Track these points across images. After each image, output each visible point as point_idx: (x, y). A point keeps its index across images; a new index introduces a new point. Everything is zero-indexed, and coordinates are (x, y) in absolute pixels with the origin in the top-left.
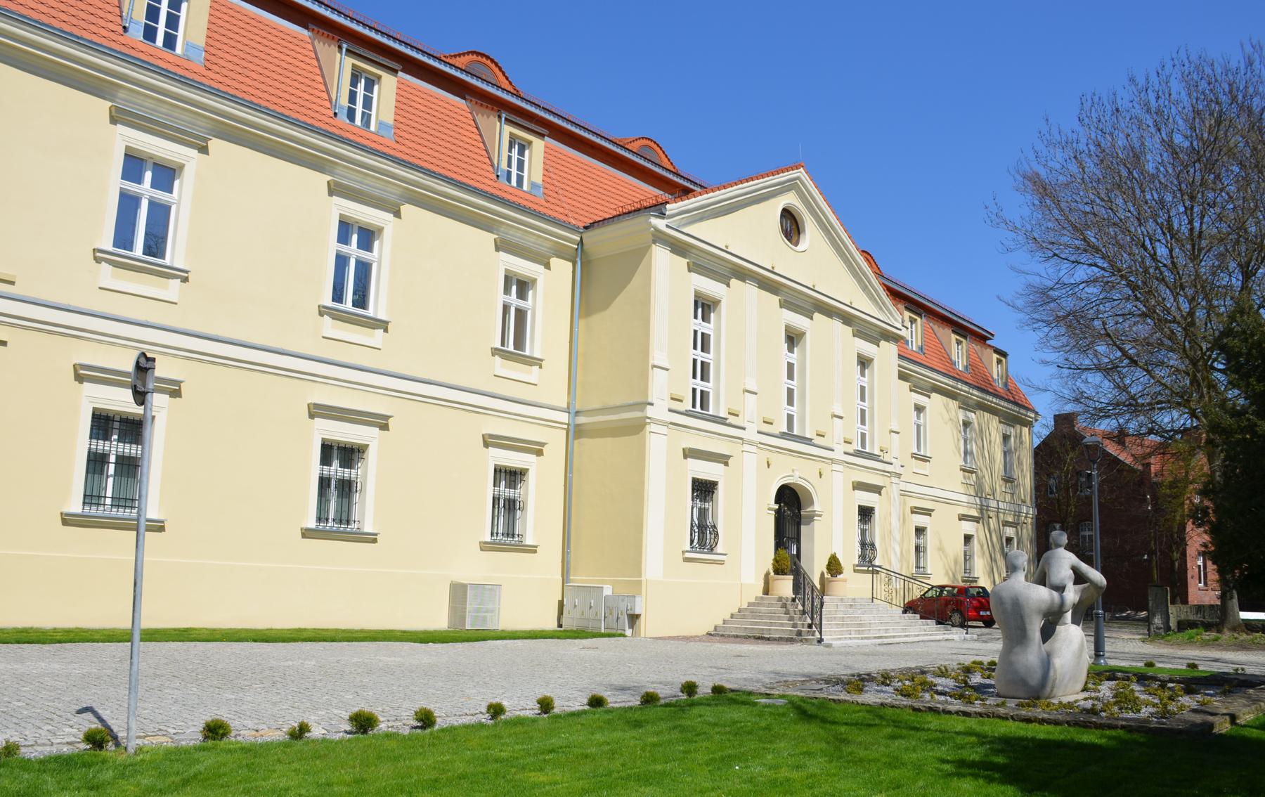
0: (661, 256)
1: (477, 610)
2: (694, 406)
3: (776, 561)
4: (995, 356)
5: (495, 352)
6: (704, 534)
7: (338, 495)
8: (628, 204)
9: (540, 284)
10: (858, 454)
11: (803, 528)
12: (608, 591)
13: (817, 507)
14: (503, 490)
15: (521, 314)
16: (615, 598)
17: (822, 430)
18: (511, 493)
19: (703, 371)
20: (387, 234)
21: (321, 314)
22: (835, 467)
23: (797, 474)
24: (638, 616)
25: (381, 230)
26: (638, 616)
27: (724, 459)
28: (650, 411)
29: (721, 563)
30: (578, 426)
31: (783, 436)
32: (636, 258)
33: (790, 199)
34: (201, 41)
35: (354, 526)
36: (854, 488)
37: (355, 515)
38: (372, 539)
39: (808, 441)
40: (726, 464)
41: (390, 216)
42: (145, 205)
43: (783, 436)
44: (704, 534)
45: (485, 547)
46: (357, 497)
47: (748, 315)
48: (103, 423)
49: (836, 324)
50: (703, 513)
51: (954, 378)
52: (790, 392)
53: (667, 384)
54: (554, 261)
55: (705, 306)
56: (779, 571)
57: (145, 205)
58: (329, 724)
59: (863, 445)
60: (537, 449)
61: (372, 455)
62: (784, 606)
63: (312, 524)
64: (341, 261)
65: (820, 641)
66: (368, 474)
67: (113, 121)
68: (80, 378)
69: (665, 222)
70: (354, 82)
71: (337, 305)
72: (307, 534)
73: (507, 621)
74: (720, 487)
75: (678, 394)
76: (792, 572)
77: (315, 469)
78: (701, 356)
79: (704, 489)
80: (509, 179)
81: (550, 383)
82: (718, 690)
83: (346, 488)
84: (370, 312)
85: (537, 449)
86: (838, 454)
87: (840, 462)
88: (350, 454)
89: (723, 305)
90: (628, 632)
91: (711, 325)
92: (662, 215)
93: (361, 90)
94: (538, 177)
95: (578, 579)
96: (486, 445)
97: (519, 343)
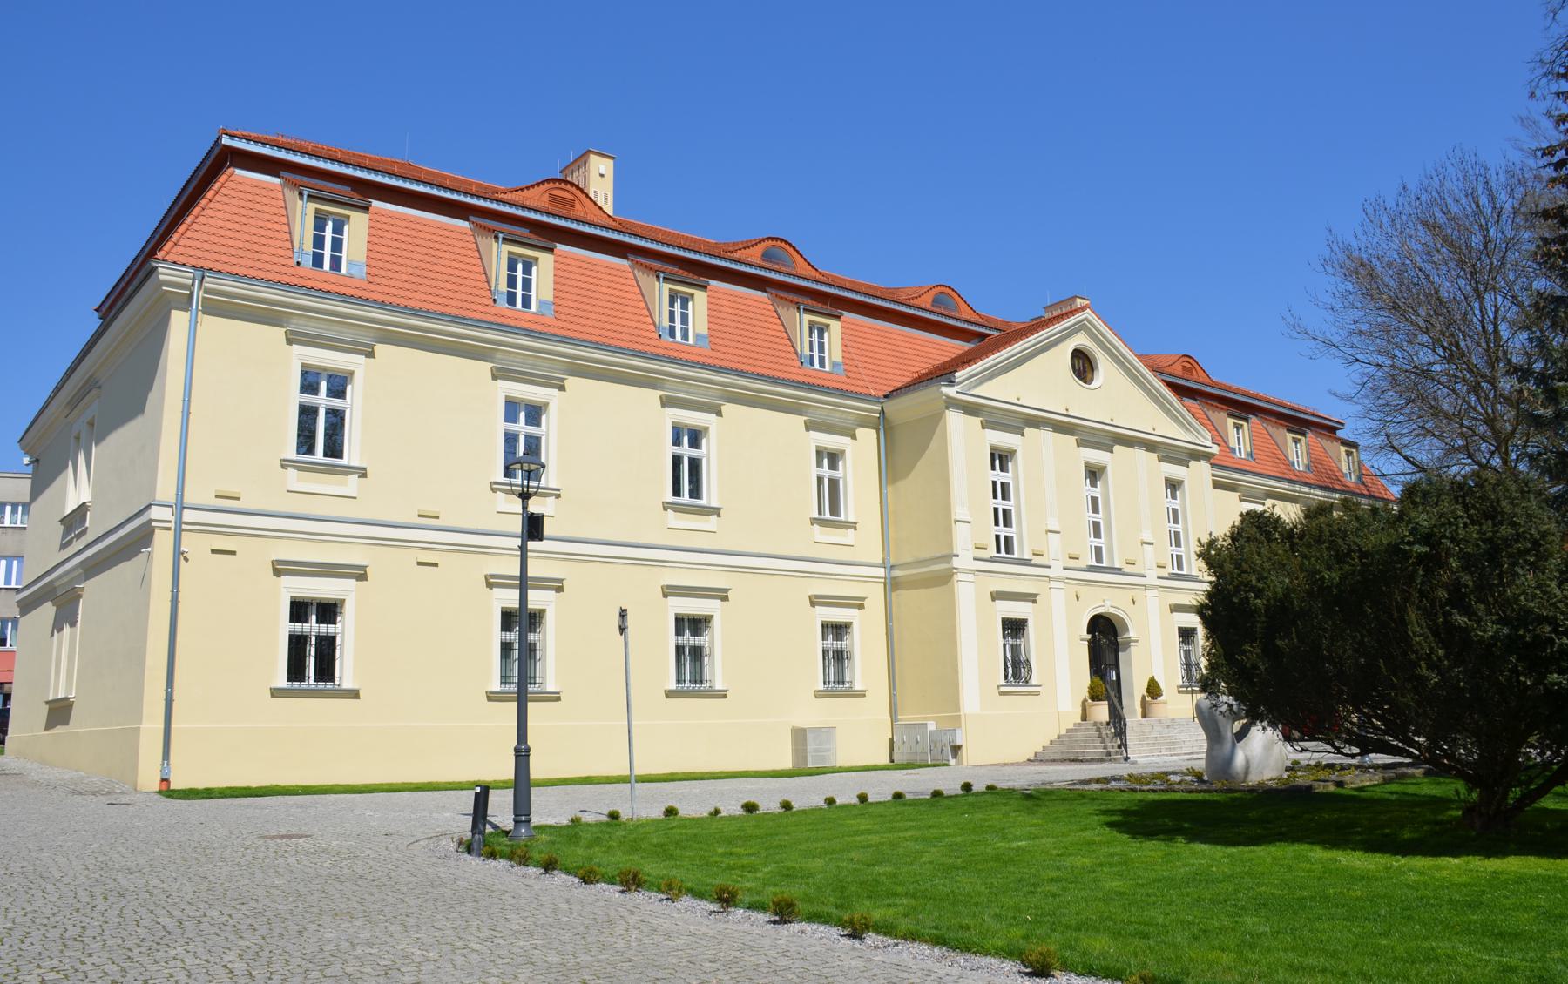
0: (956, 422)
1: (816, 751)
2: (998, 551)
3: (1091, 688)
4: (1343, 449)
5: (814, 521)
6: (1017, 668)
7: (692, 659)
8: (924, 366)
9: (848, 455)
10: (1173, 577)
11: (1121, 654)
12: (931, 726)
13: (1132, 633)
14: (832, 644)
15: (834, 484)
16: (938, 731)
17: (1131, 558)
18: (839, 645)
19: (1006, 518)
20: (712, 433)
21: (665, 509)
22: (1149, 592)
23: (1108, 603)
24: (960, 747)
25: (707, 429)
26: (960, 747)
27: (1031, 598)
28: (956, 562)
29: (1037, 694)
30: (894, 579)
31: (1091, 569)
32: (933, 422)
33: (1080, 340)
34: (549, 297)
35: (706, 685)
36: (1172, 611)
37: (707, 676)
38: (722, 695)
39: (1118, 571)
40: (1034, 602)
41: (713, 417)
42: (522, 439)
43: (1091, 569)
44: (1017, 668)
45: (819, 695)
46: (706, 660)
47: (1046, 461)
48: (508, 619)
49: (1140, 453)
50: (1015, 649)
51: (1289, 481)
52: (1096, 525)
53: (971, 532)
54: (860, 432)
55: (1001, 458)
56: (1095, 697)
57: (522, 439)
58: (732, 808)
59: (1180, 567)
60: (858, 604)
61: (717, 623)
62: (1098, 730)
63: (673, 686)
64: (677, 461)
65: (1127, 759)
66: (716, 640)
67: (495, 378)
68: (490, 585)
69: (956, 388)
70: (672, 304)
71: (677, 499)
72: (670, 694)
73: (841, 761)
74: (1030, 624)
75: (981, 543)
76: (1108, 698)
77: (672, 640)
78: (1001, 504)
79: (1014, 628)
80: (812, 363)
81: (865, 543)
82: (991, 788)
83: (697, 653)
84: (704, 501)
85: (858, 604)
86: (1151, 579)
87: (1154, 587)
88: (697, 624)
89: (1020, 455)
90: (952, 762)
91: (1010, 474)
92: (951, 383)
93: (678, 304)
94: (838, 358)
95: (905, 717)
96: (813, 604)
97: (835, 510)
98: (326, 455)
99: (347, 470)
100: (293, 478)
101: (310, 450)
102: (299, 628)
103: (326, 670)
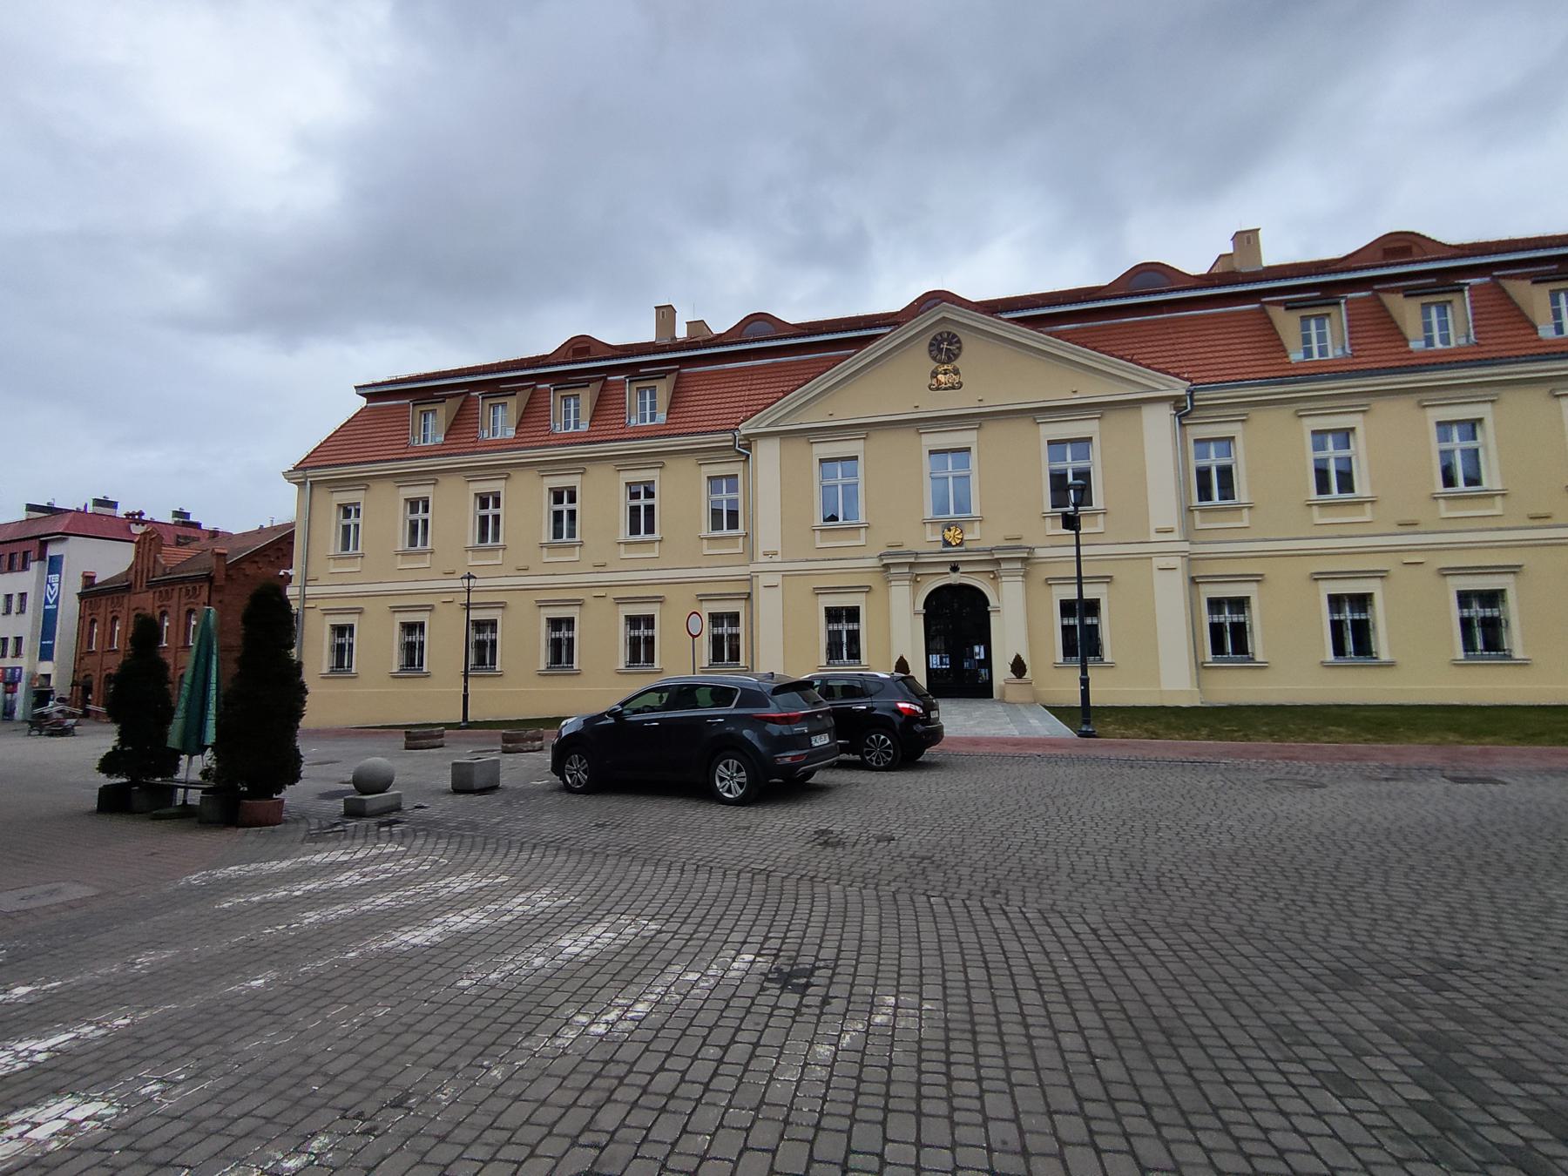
98: (1340, 491)
99: (1490, 496)
100: (1317, 516)
101: (1209, 498)
102: (1466, 613)
103: (1241, 647)
